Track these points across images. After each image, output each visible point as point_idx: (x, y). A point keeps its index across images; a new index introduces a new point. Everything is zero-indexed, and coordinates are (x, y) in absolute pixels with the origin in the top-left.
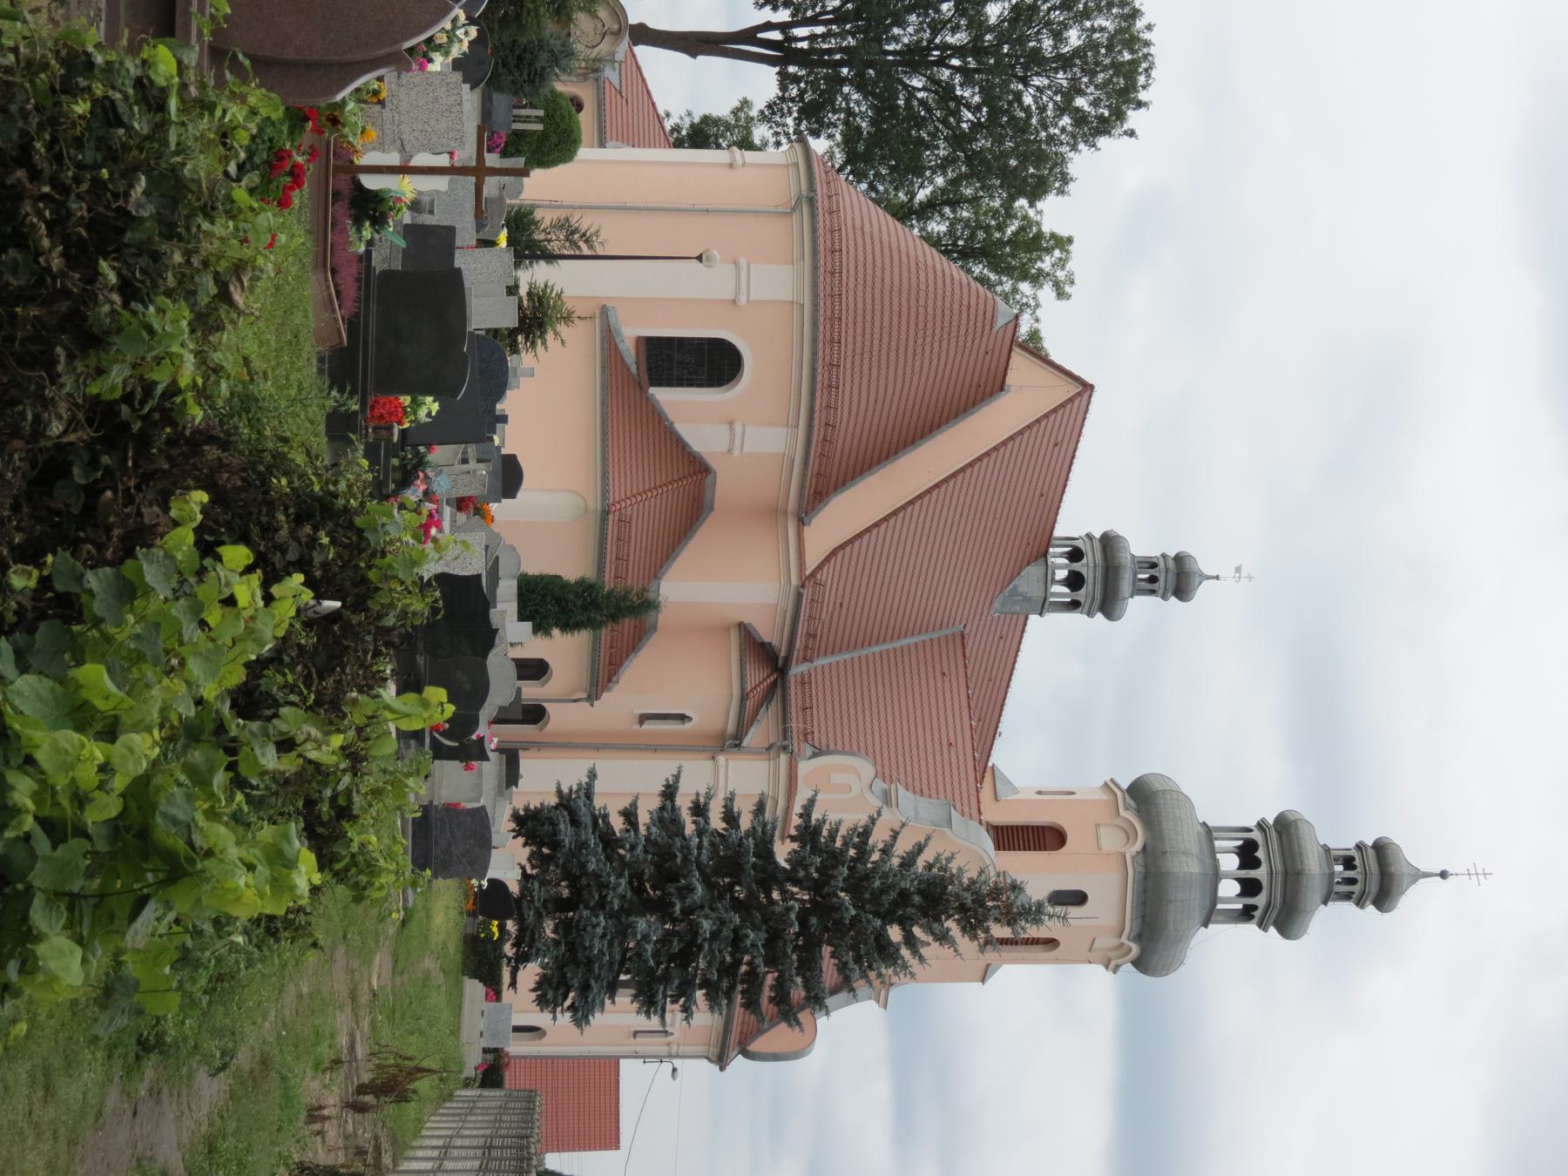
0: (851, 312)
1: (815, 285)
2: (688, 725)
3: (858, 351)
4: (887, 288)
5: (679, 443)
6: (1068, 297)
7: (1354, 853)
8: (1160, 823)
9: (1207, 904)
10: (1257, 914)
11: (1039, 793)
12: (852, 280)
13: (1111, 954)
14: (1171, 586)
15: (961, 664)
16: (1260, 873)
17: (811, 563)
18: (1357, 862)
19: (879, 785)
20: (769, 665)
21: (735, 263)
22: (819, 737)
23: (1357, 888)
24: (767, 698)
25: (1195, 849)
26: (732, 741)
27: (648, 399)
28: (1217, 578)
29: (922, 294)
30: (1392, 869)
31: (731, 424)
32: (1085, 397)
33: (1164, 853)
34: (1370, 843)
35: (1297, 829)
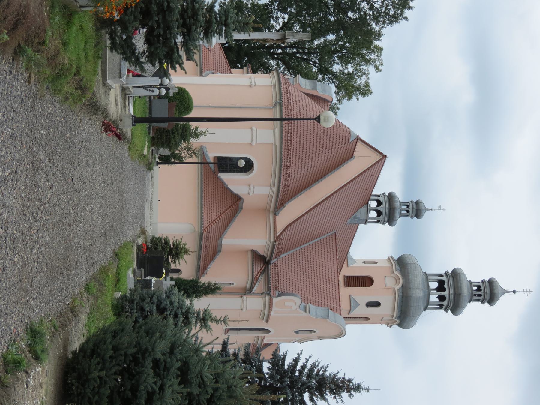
0: (295, 145)
1: (281, 139)
2: (232, 286)
3: (297, 159)
4: (309, 134)
5: (230, 192)
6: (380, 71)
7: (481, 284)
8: (408, 276)
9: (425, 305)
10: (444, 307)
11: (364, 262)
12: (295, 133)
13: (389, 322)
14: (414, 214)
15: (334, 246)
16: (446, 294)
17: (279, 230)
18: (482, 288)
19: (303, 304)
20: (262, 261)
21: (249, 187)
22: (281, 288)
23: (481, 298)
24: (262, 273)
25: (421, 286)
26: (248, 291)
27: (218, 178)
28: (432, 210)
29: (322, 134)
30: (495, 292)
31: (249, 186)
32: (383, 160)
33: (410, 288)
34: (487, 280)
35: (460, 276)
